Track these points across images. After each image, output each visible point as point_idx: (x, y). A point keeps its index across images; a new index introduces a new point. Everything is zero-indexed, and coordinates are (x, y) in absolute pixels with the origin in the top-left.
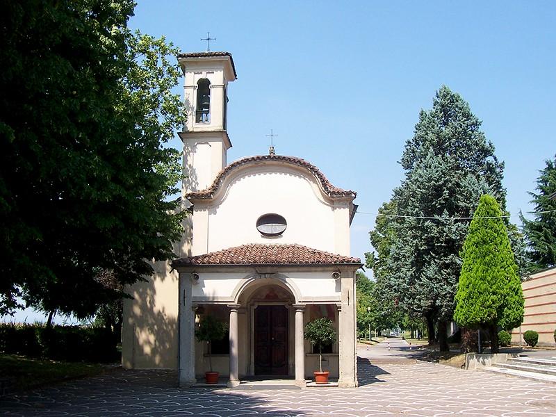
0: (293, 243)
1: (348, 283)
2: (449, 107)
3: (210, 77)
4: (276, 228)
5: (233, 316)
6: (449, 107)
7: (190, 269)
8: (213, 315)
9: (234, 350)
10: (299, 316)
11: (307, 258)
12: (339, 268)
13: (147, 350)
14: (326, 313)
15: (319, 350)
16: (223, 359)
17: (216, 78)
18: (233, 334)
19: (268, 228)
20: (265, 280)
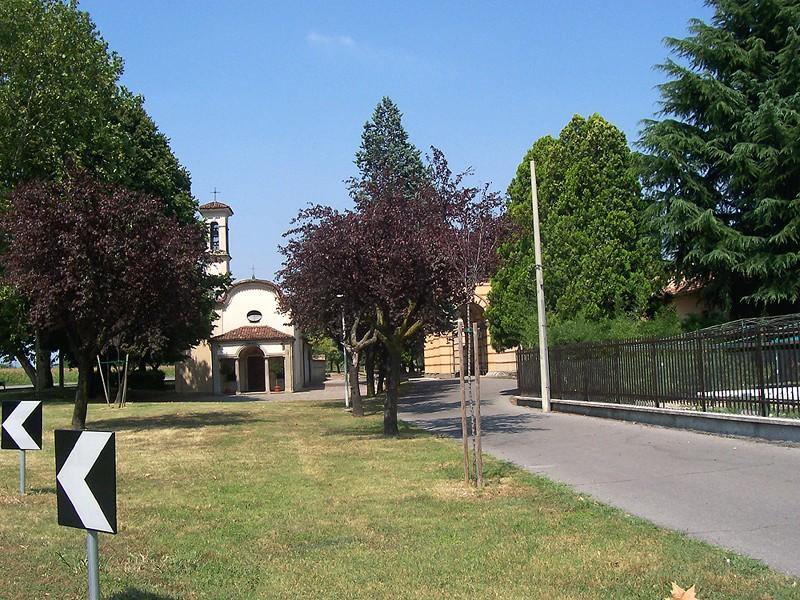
0: (163, 129)
1: (288, 347)
2: (387, 103)
3: (217, 220)
4: (257, 318)
5: (237, 363)
6: (387, 118)
7: (216, 343)
8: (225, 365)
9: (238, 378)
10: (266, 362)
11: (270, 335)
12: (283, 340)
13: (188, 382)
14: (278, 361)
15: (74, 397)
16: (232, 383)
17: (221, 221)
18: (237, 373)
19: (252, 318)
20: (250, 346)
